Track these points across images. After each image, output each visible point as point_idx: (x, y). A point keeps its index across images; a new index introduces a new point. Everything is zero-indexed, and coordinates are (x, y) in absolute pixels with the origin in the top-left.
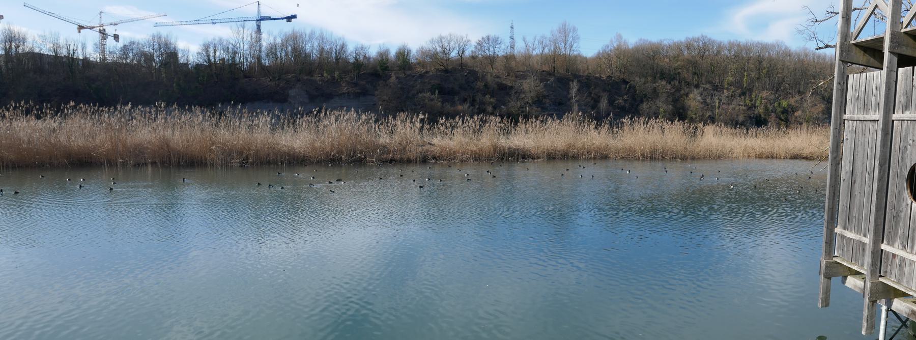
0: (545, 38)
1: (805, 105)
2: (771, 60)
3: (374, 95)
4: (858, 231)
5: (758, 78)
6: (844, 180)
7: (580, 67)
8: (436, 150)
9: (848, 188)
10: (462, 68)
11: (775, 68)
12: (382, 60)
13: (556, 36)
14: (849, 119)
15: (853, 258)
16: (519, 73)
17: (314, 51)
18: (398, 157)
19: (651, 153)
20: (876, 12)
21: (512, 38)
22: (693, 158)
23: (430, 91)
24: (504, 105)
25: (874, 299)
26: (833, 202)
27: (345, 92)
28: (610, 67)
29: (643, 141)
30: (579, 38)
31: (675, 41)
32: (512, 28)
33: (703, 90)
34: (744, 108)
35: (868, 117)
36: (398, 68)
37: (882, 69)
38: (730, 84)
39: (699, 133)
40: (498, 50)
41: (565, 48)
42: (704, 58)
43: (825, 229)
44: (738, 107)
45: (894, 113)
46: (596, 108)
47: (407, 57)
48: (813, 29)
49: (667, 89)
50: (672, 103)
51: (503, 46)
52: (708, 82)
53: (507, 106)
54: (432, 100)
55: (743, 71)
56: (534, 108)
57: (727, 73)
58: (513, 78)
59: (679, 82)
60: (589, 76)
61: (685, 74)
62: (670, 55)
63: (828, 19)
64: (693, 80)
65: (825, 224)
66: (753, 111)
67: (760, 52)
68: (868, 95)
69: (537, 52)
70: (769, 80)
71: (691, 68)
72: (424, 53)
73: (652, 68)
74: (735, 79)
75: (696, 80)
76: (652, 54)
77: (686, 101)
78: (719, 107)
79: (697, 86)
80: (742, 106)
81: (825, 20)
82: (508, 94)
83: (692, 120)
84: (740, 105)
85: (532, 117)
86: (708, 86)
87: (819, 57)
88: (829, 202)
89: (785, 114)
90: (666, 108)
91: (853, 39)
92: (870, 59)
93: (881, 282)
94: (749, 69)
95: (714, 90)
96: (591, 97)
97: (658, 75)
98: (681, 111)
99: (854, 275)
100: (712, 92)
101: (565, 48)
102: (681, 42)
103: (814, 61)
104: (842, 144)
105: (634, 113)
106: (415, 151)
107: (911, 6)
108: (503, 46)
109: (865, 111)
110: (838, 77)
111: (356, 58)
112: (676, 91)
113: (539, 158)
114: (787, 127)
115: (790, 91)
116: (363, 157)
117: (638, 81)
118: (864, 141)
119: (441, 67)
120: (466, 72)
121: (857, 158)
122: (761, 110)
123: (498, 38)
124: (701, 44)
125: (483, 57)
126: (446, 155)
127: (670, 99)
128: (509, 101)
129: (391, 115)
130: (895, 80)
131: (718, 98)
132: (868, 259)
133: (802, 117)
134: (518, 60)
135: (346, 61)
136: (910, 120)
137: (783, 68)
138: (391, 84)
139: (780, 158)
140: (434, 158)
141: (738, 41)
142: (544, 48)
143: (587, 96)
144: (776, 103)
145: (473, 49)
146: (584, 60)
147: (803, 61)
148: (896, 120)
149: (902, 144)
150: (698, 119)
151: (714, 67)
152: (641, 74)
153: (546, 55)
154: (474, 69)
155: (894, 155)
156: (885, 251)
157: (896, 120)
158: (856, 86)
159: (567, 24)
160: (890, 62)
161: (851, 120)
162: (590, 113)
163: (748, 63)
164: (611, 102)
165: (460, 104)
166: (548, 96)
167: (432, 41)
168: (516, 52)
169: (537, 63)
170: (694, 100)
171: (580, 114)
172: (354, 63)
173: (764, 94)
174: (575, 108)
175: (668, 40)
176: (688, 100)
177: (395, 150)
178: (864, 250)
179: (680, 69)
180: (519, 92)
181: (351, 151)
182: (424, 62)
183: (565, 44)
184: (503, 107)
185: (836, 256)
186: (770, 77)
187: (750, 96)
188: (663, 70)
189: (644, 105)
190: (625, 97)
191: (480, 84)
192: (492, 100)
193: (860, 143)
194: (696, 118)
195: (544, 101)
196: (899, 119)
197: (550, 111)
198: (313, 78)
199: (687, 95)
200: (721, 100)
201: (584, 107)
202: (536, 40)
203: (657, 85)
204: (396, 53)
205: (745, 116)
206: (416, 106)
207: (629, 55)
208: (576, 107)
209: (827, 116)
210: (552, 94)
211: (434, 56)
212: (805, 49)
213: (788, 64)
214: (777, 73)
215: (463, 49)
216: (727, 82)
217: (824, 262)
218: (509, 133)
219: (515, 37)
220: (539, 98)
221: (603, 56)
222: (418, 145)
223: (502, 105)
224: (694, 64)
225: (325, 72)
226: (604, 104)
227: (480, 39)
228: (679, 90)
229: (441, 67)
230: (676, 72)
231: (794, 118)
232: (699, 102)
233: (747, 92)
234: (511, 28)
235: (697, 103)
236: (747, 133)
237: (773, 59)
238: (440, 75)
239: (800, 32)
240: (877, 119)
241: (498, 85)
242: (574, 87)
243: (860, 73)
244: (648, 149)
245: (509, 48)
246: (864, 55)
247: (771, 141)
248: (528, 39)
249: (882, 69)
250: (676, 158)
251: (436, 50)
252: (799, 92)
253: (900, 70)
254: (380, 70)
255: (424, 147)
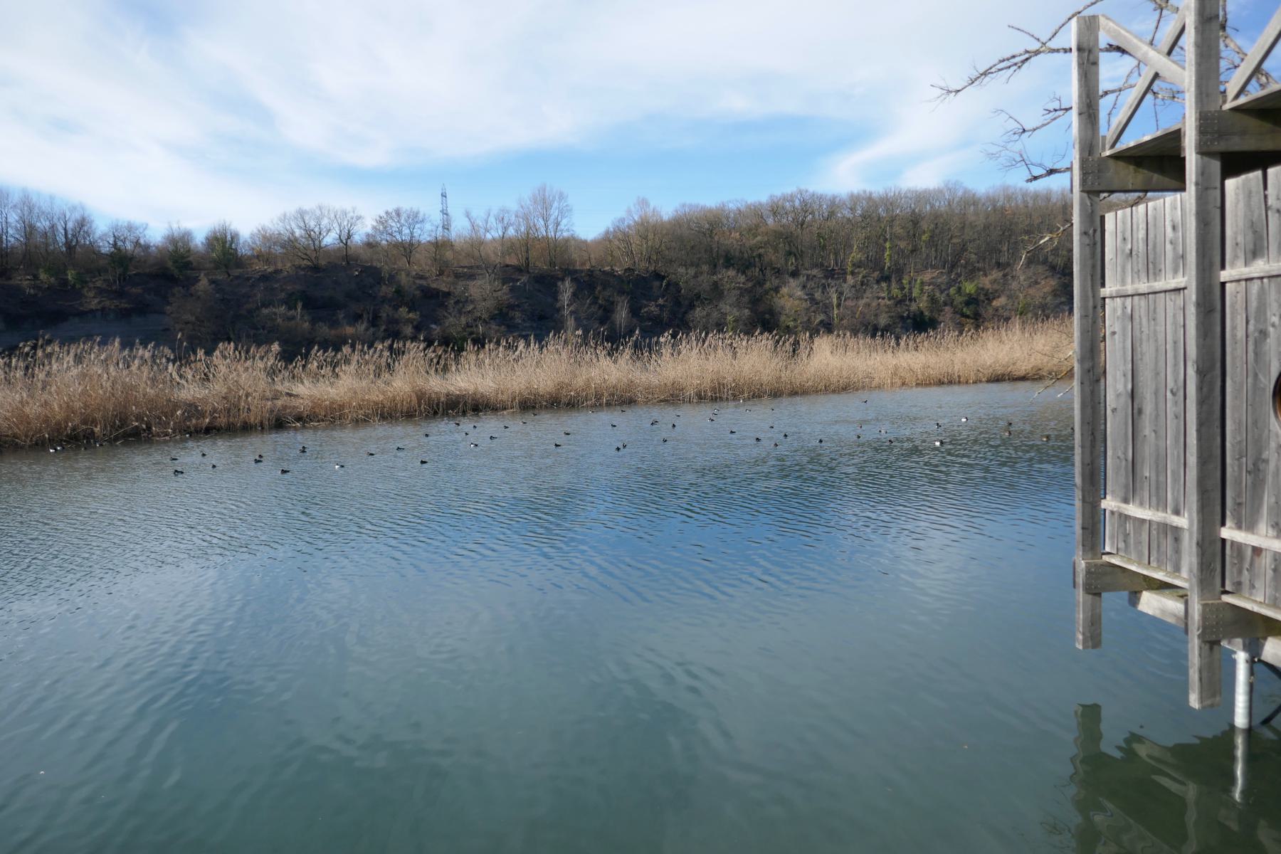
0: (508, 212)
1: (1014, 285)
2: (936, 216)
3: (163, 313)
4: (1158, 505)
5: (912, 251)
6: (1114, 410)
7: (575, 256)
8: (302, 405)
9: (1126, 423)
10: (348, 263)
11: (946, 228)
12: (176, 251)
13: (528, 208)
14: (1114, 295)
15: (1152, 554)
16: (461, 269)
17: (11, 231)
18: (222, 421)
19: (713, 389)
20: (1155, 87)
21: (445, 213)
22: (794, 393)
23: (286, 303)
24: (435, 323)
25: (1214, 638)
26: (1092, 453)
27: (93, 307)
28: (630, 253)
29: (698, 371)
30: (571, 210)
31: (749, 202)
32: (444, 195)
33: (808, 279)
34: (888, 303)
35: (1159, 285)
36: (212, 265)
37: (1183, 189)
38: (858, 265)
39: (803, 352)
40: (419, 232)
41: (546, 227)
42: (804, 226)
43: (1078, 503)
44: (877, 300)
45: (1223, 267)
46: (608, 322)
47: (231, 245)
48: (1017, 147)
49: (739, 283)
50: (749, 306)
51: (428, 226)
52: (816, 266)
53: (440, 324)
54: (293, 318)
55: (881, 241)
56: (494, 327)
57: (851, 247)
58: (450, 279)
59: (761, 270)
60: (592, 271)
61: (771, 256)
62: (740, 227)
63: (1048, 123)
64: (787, 264)
65: (1078, 494)
66: (907, 305)
67: (913, 206)
68: (1155, 246)
69: (494, 234)
70: (936, 251)
71: (781, 245)
72: (267, 239)
73: (709, 250)
74: (866, 255)
75: (792, 263)
76: (707, 226)
77: (775, 300)
78: (839, 305)
79: (795, 274)
80: (884, 298)
81: (1044, 125)
82: (443, 305)
83: (788, 330)
84: (879, 298)
85: (490, 342)
86: (815, 272)
87: (1036, 196)
88: (1083, 453)
89: (972, 307)
90: (737, 314)
91: (1107, 146)
92: (1152, 177)
93: (1228, 603)
94: (895, 237)
95: (826, 277)
96: (597, 306)
97: (721, 261)
98: (767, 316)
99: (1157, 589)
100: (824, 281)
101: (546, 227)
102: (760, 204)
103: (1027, 207)
104: (1102, 344)
105: (678, 326)
106: (258, 409)
107: (1241, 56)
108: (428, 226)
109: (1151, 271)
110: (1082, 222)
111: (115, 245)
112: (755, 286)
113: (505, 409)
114: (977, 327)
115: (980, 265)
116: (144, 426)
117: (682, 274)
118: (1155, 331)
119: (305, 262)
120: (356, 270)
121: (1141, 367)
122: (923, 304)
123: (418, 213)
124: (797, 203)
125: (389, 244)
126: (323, 413)
127: (746, 299)
128: (444, 316)
129: (201, 349)
130: (1219, 204)
131: (837, 291)
132: (1189, 558)
133: (1008, 307)
134: (458, 248)
135: (92, 250)
136: (1270, 277)
137: (963, 227)
138: (200, 293)
139: (967, 382)
140: (299, 418)
141: (868, 192)
142: (505, 229)
143: (590, 304)
144: (951, 289)
145: (369, 230)
146: (583, 245)
147: (1003, 208)
148: (1231, 282)
149: (1251, 327)
150: (800, 328)
151: (824, 240)
152: (689, 262)
153: (510, 238)
154: (375, 264)
155: (1234, 349)
156: (1233, 542)
157: (1231, 282)
158: (1123, 232)
159: (548, 189)
160: (1203, 173)
161: (1120, 297)
162: (598, 330)
163: (891, 227)
164: (634, 312)
165: (350, 324)
166: (518, 306)
167: (284, 218)
168: (453, 235)
169: (496, 254)
170: (790, 298)
171: (579, 332)
172: (111, 255)
173: (927, 276)
174: (569, 323)
175: (737, 201)
176: (780, 298)
177: (215, 410)
178: (1177, 540)
179: (761, 247)
180: (462, 302)
181: (116, 416)
182: (270, 253)
183: (546, 221)
184: (433, 326)
185: (1109, 553)
186: (937, 245)
187: (900, 281)
188: (729, 251)
189: (697, 312)
190: (661, 301)
191: (386, 290)
192: (411, 315)
193: (1144, 337)
194: (796, 327)
195: (511, 313)
196: (1237, 278)
197: (522, 330)
198: (12, 282)
199: (777, 290)
200: (841, 293)
201: (585, 322)
202: (491, 214)
203: (720, 276)
204: (207, 238)
205: (891, 317)
206: (257, 329)
207: (664, 232)
208: (571, 322)
209: (1063, 299)
210: (526, 302)
211: (290, 244)
212: (1006, 188)
213: (973, 219)
214: (951, 238)
215: (349, 231)
216: (852, 261)
217: (1082, 564)
218: (446, 369)
219: (449, 211)
220: (501, 310)
221: (615, 237)
222: (264, 398)
223: (432, 323)
224: (787, 238)
225: (41, 270)
226: (622, 315)
227: (383, 214)
228: (760, 283)
229: (305, 262)
230: (755, 254)
231: (991, 311)
232: (800, 299)
233: (893, 276)
234: (442, 195)
235: (797, 302)
236: (898, 344)
237: (942, 215)
238: (305, 275)
239: (991, 156)
240: (1182, 285)
241: (423, 291)
242: (566, 290)
243: (1132, 206)
244: (707, 384)
245: (440, 229)
246: (1135, 172)
247: (948, 355)
248: (474, 214)
249: (1183, 189)
250: (760, 397)
251: (293, 233)
252: (999, 265)
253: (1231, 183)
254: (172, 268)
255: (276, 401)
